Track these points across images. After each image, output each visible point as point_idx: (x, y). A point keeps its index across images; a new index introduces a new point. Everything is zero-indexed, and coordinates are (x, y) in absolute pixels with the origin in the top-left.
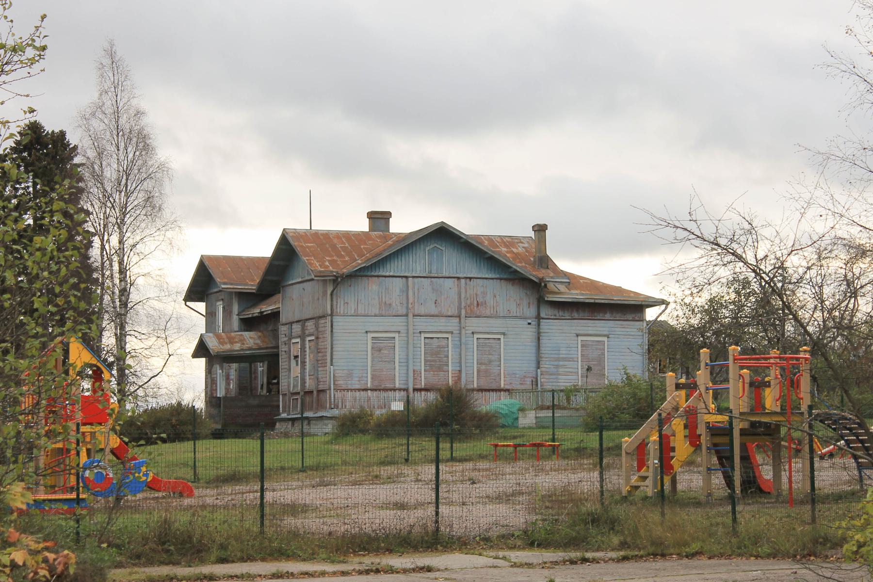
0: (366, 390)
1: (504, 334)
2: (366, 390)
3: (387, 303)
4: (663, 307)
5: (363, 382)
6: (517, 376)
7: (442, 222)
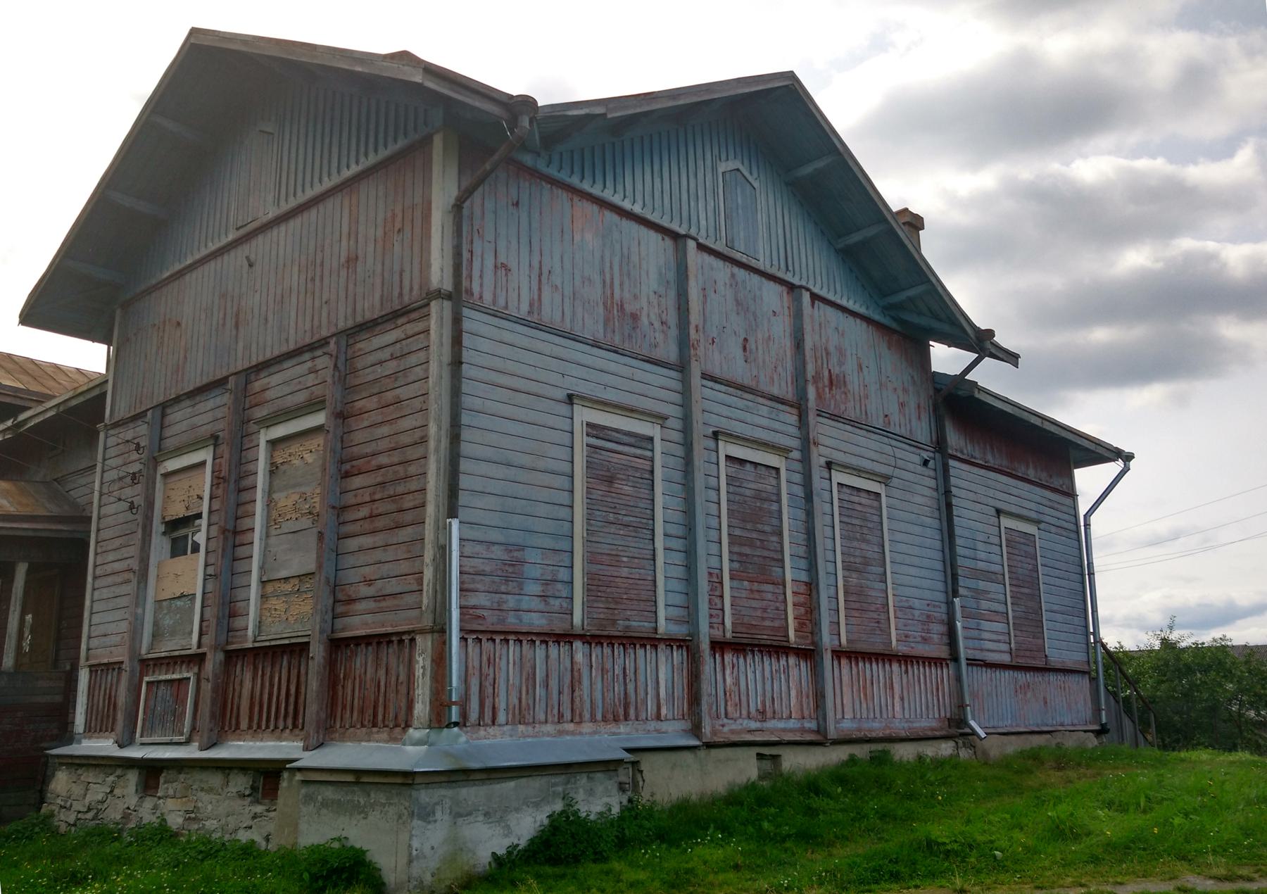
0: (565, 638)
1: (885, 479)
2: (565, 638)
3: (628, 308)
4: (1114, 468)
5: (556, 603)
6: (917, 613)
7: (791, 75)
